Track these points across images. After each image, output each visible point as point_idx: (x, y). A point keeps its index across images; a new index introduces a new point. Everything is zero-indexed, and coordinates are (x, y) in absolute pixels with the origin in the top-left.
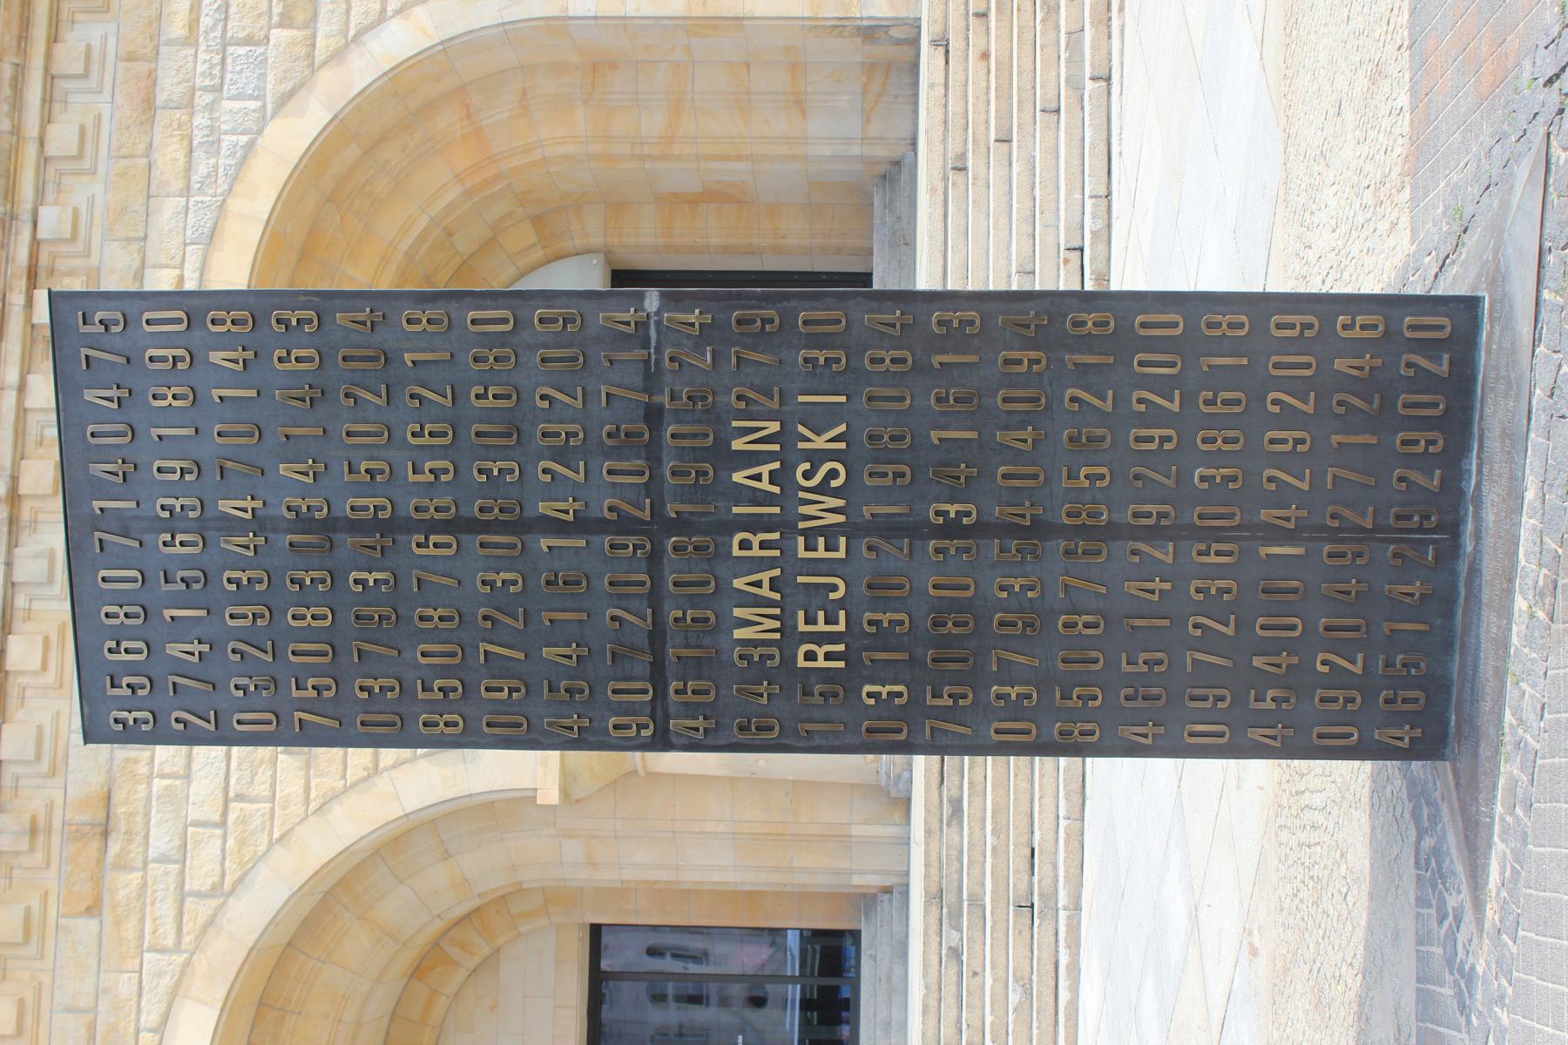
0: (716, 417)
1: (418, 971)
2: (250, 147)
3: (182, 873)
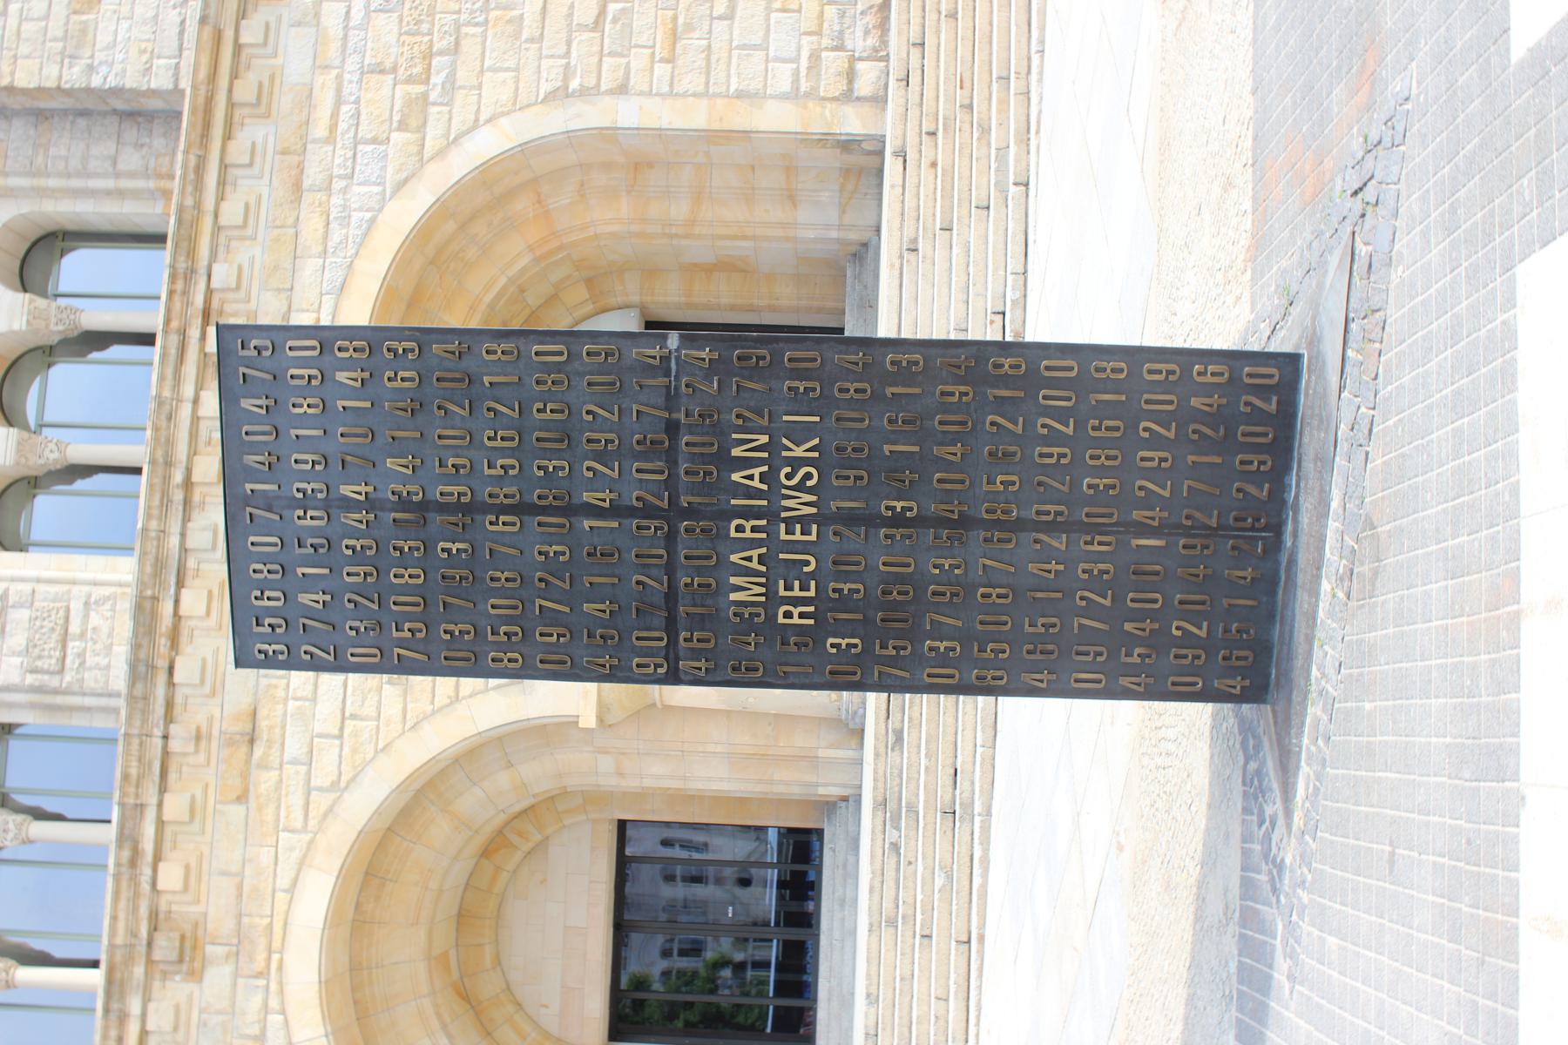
0: (720, 431)
1: (486, 852)
2: (373, 220)
3: (309, 773)
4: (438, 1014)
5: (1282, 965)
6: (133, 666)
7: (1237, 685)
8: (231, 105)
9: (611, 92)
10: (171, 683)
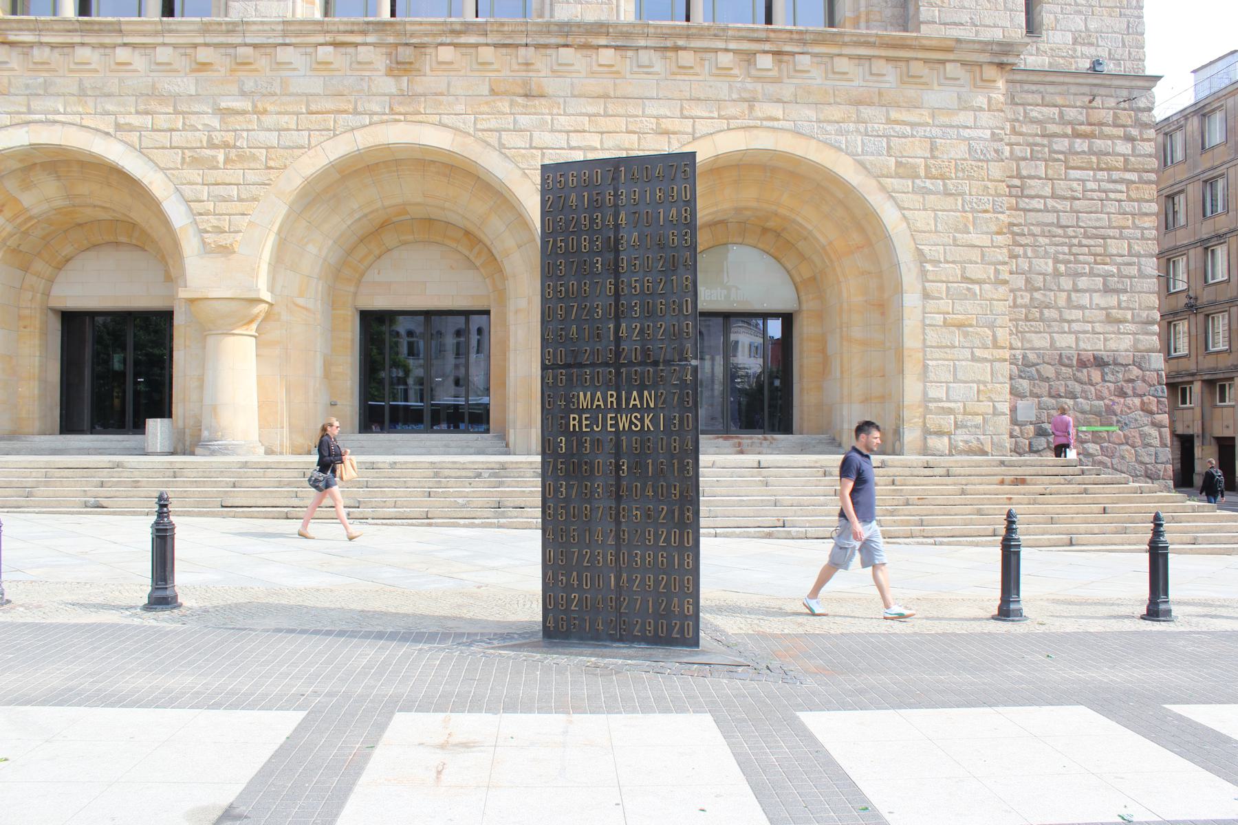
0: (655, 385)
1: (467, 233)
2: (840, 149)
3: (509, 130)
4: (372, 212)
5: (426, 647)
6: (567, 24)
7: (551, 625)
8: (908, 60)
9: (924, 289)
10: (558, 46)
